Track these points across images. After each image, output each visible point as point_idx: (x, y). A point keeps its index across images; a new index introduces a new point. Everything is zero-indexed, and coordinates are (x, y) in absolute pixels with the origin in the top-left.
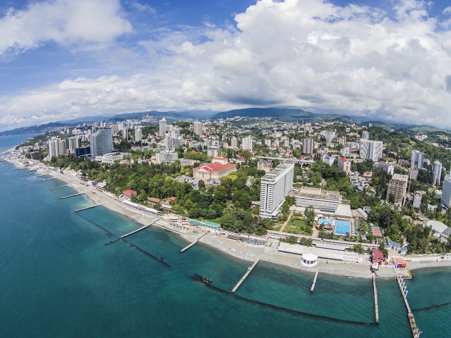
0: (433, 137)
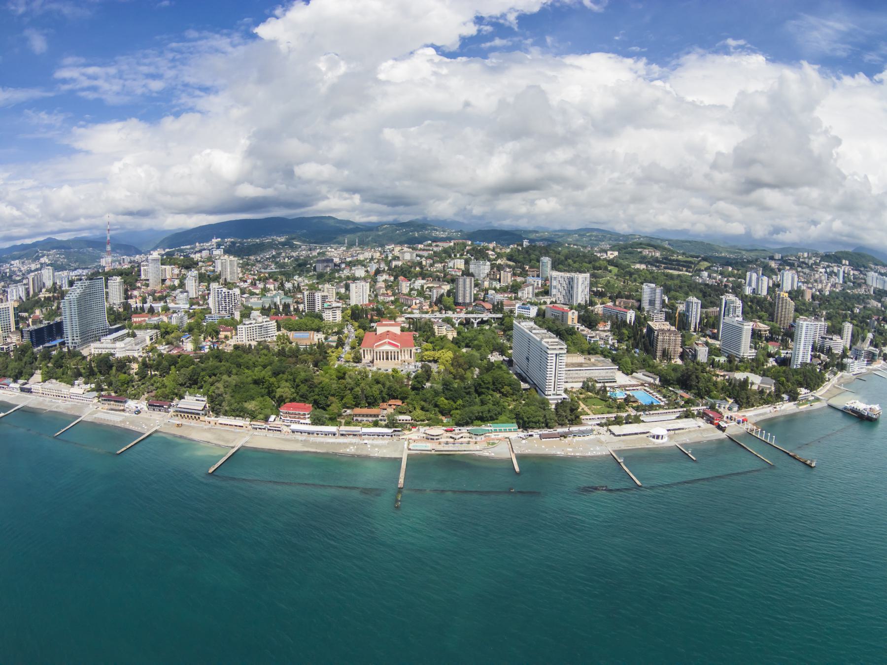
0: (630, 253)
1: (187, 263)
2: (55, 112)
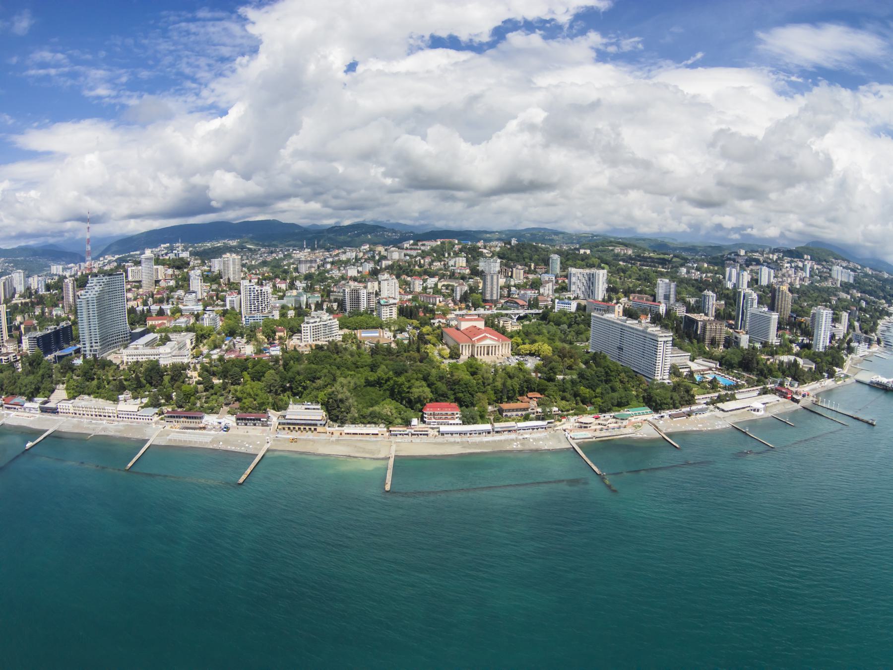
1: (177, 263)
2: (172, 90)
